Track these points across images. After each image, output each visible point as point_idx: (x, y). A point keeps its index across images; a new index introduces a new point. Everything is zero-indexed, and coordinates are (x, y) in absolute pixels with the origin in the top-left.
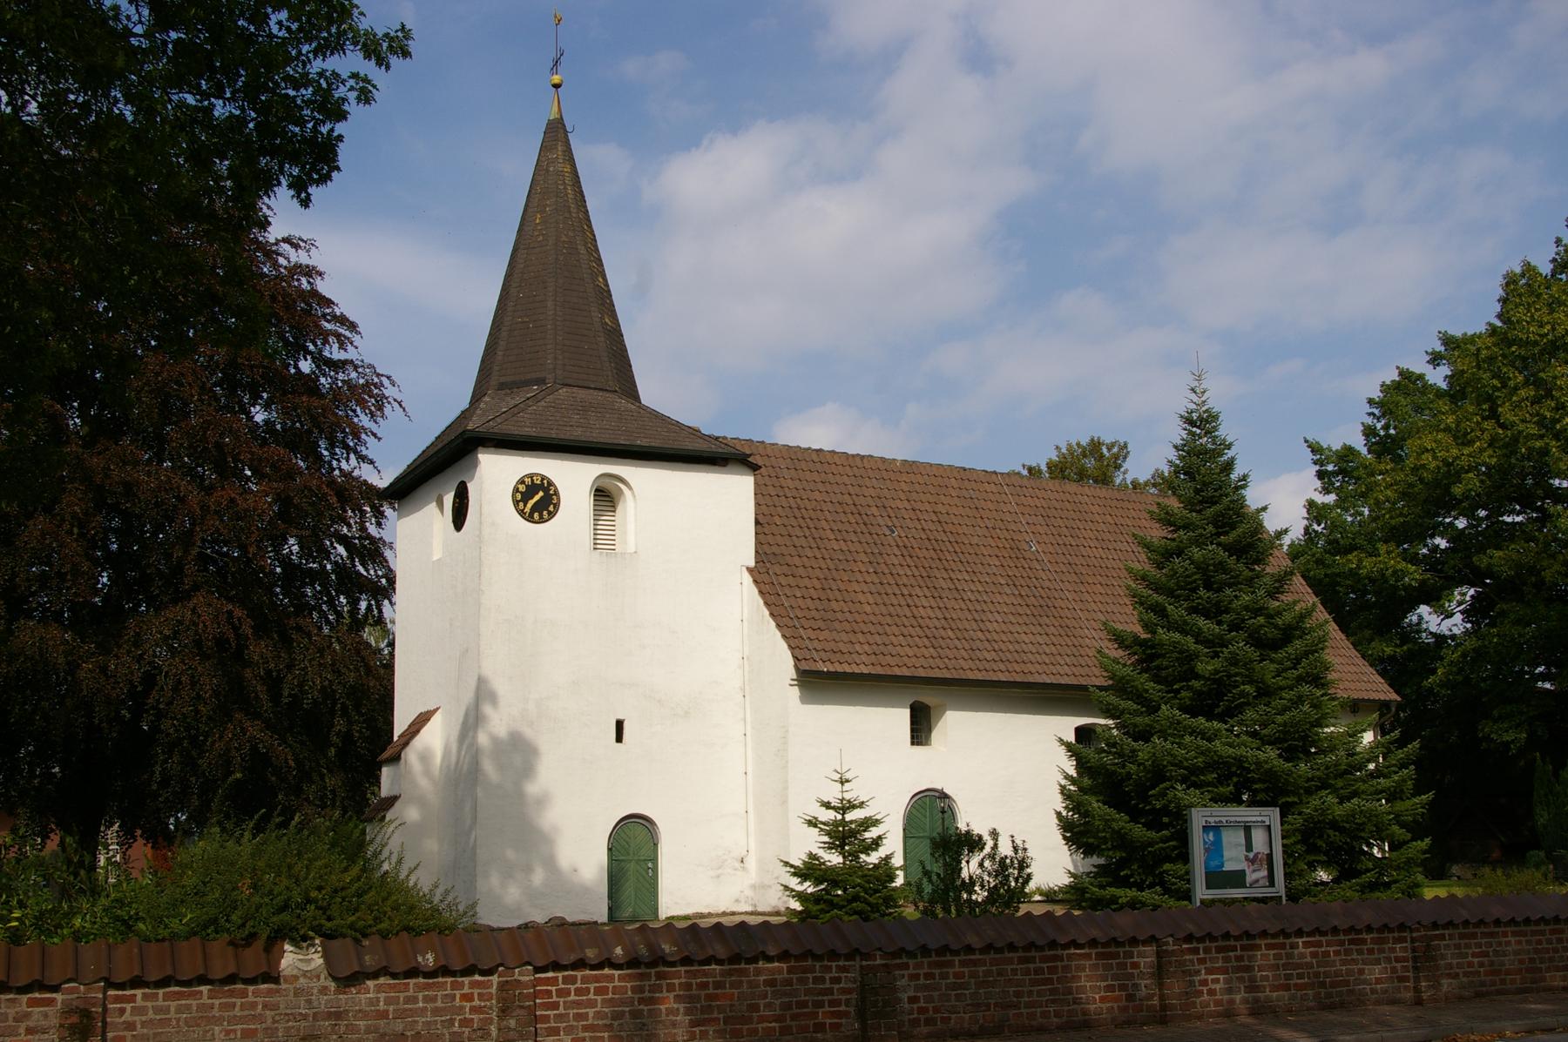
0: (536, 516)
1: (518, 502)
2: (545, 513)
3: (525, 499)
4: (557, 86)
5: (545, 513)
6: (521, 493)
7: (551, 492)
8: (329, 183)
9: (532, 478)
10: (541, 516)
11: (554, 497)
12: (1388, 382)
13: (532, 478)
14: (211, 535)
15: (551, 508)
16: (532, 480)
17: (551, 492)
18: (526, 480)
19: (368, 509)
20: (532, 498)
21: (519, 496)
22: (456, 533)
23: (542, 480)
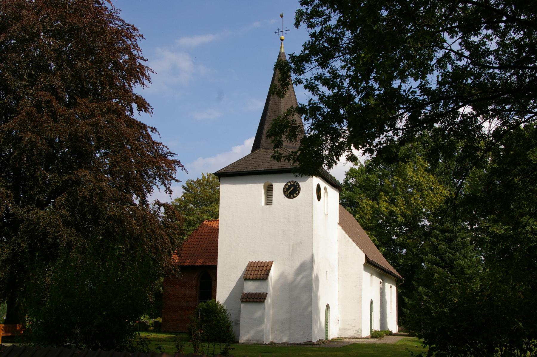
0: (292, 196)
1: (285, 192)
2: (295, 194)
3: (287, 191)
4: (282, 40)
5: (295, 194)
6: (286, 188)
7: (297, 187)
8: (331, 19)
9: (290, 182)
10: (293, 196)
11: (298, 188)
12: (335, 178)
13: (290, 182)
14: (106, 92)
15: (297, 192)
16: (291, 183)
17: (297, 187)
18: (288, 183)
19: (532, 66)
20: (290, 190)
21: (286, 190)
22: (273, 206)
23: (294, 182)
